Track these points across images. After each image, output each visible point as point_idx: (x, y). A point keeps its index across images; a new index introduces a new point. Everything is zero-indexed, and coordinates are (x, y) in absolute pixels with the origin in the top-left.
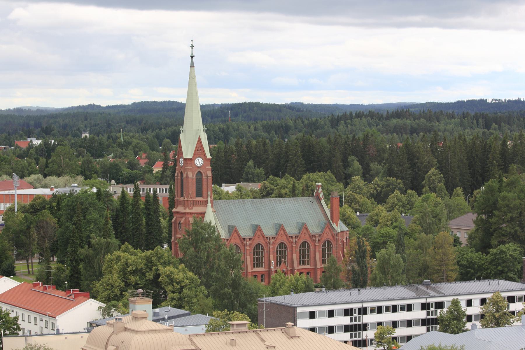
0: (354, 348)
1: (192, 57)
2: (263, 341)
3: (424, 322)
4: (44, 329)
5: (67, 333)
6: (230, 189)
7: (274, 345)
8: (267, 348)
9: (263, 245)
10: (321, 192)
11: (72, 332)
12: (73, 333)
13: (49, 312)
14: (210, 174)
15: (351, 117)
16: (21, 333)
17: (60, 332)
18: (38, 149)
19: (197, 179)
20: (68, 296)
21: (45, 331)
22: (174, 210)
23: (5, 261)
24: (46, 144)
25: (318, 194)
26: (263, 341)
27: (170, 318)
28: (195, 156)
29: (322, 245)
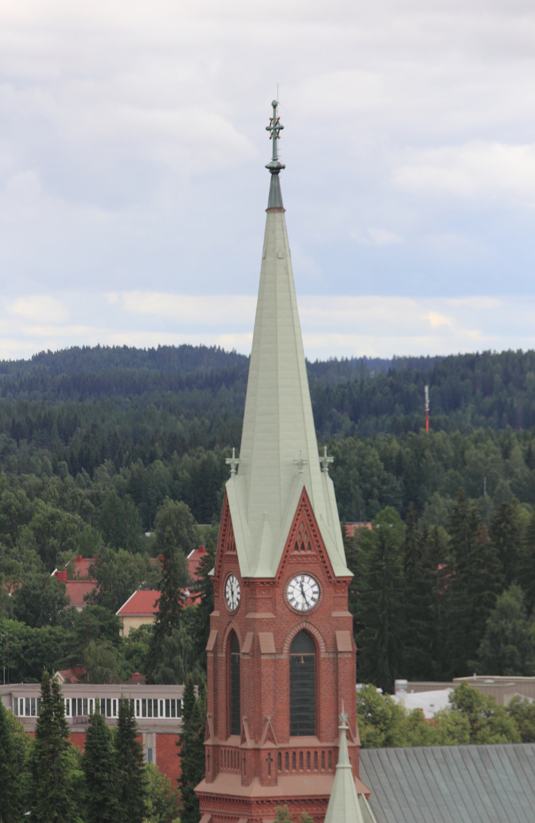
1: (275, 170)
19: (294, 661)
22: (202, 787)
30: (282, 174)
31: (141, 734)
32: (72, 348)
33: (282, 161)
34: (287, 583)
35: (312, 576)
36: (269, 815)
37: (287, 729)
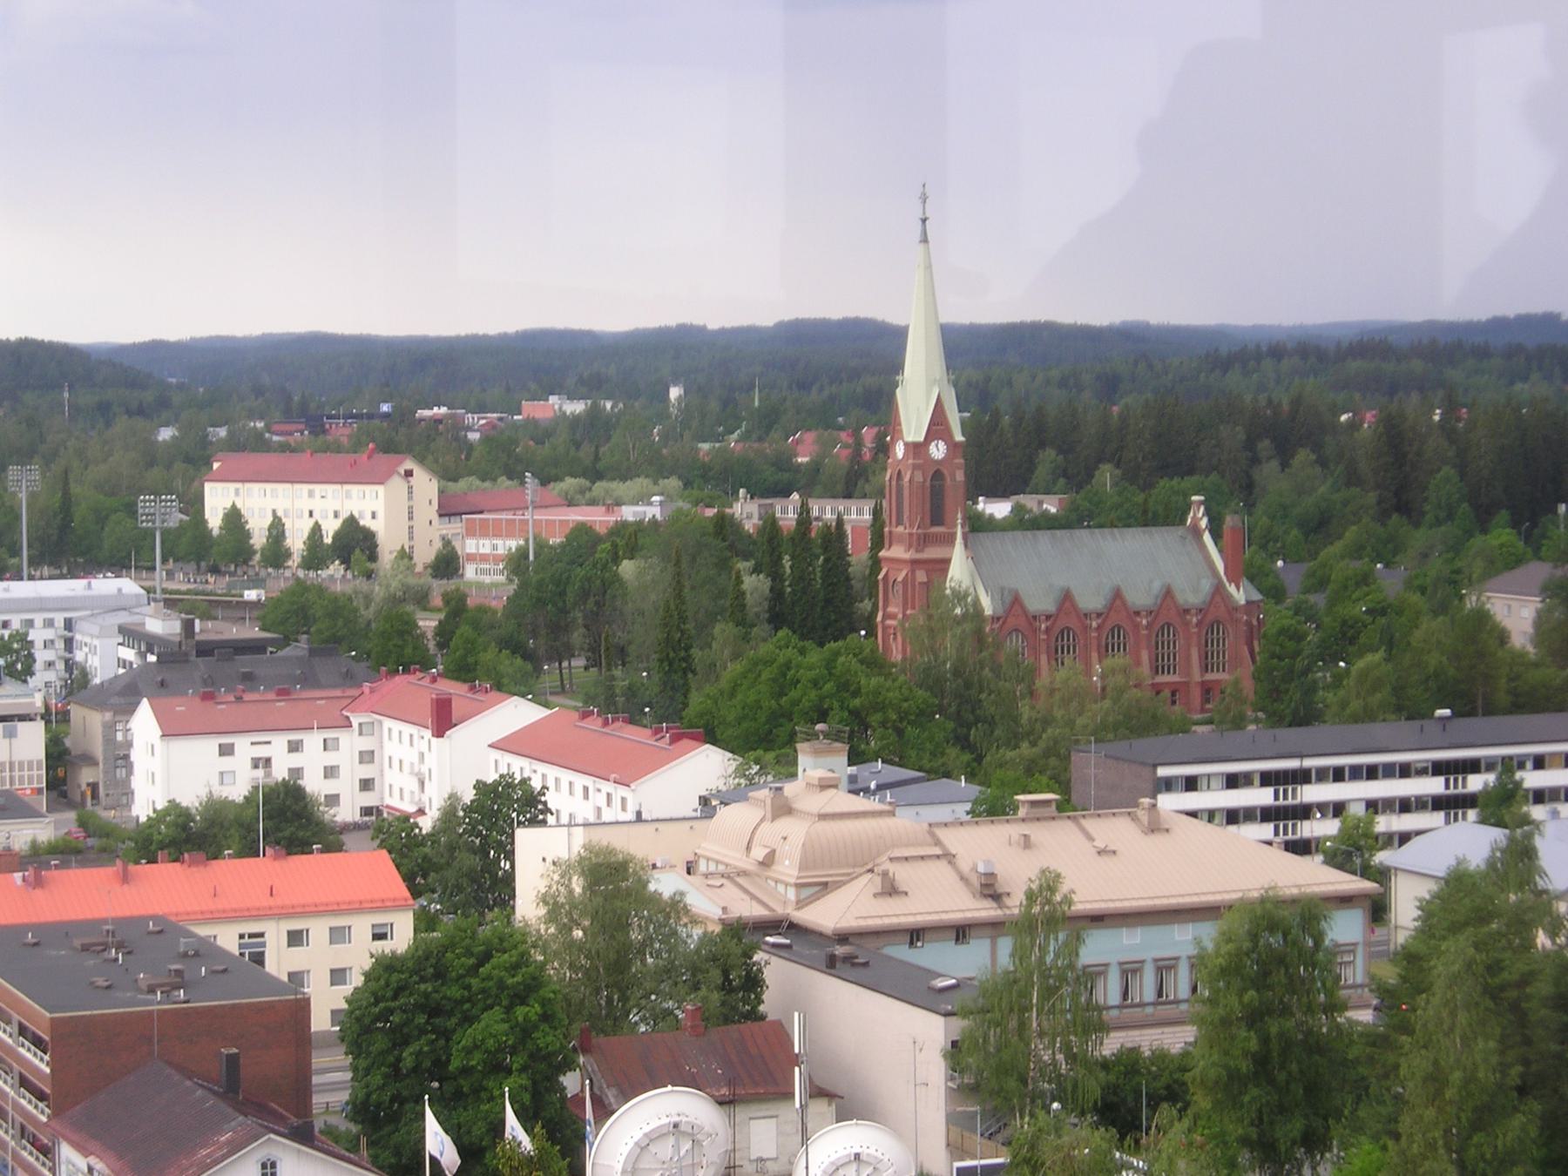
0: (1289, 855)
1: (924, 221)
2: (1091, 838)
3: (1438, 803)
4: (605, 810)
5: (658, 820)
6: (1000, 509)
7: (1113, 848)
8: (1099, 853)
9: (1078, 632)
10: (1203, 515)
11: (667, 816)
12: (671, 820)
13: (613, 773)
14: (960, 476)
15: (1258, 355)
16: (551, 819)
17: (644, 817)
18: (575, 421)
19: (932, 486)
20: (657, 740)
21: (608, 816)
22: (882, 554)
23: (889, 683)
24: (594, 414)
25: (1196, 521)
26: (1091, 838)
27: (880, 788)
28: (931, 435)
29: (1204, 632)
30: (927, 222)
31: (115, 865)
32: (191, 338)
33: (927, 215)
34: (930, 444)
35: (943, 440)
36: (386, 907)
37: (929, 521)
